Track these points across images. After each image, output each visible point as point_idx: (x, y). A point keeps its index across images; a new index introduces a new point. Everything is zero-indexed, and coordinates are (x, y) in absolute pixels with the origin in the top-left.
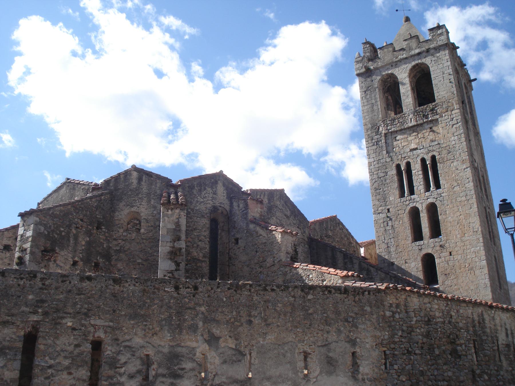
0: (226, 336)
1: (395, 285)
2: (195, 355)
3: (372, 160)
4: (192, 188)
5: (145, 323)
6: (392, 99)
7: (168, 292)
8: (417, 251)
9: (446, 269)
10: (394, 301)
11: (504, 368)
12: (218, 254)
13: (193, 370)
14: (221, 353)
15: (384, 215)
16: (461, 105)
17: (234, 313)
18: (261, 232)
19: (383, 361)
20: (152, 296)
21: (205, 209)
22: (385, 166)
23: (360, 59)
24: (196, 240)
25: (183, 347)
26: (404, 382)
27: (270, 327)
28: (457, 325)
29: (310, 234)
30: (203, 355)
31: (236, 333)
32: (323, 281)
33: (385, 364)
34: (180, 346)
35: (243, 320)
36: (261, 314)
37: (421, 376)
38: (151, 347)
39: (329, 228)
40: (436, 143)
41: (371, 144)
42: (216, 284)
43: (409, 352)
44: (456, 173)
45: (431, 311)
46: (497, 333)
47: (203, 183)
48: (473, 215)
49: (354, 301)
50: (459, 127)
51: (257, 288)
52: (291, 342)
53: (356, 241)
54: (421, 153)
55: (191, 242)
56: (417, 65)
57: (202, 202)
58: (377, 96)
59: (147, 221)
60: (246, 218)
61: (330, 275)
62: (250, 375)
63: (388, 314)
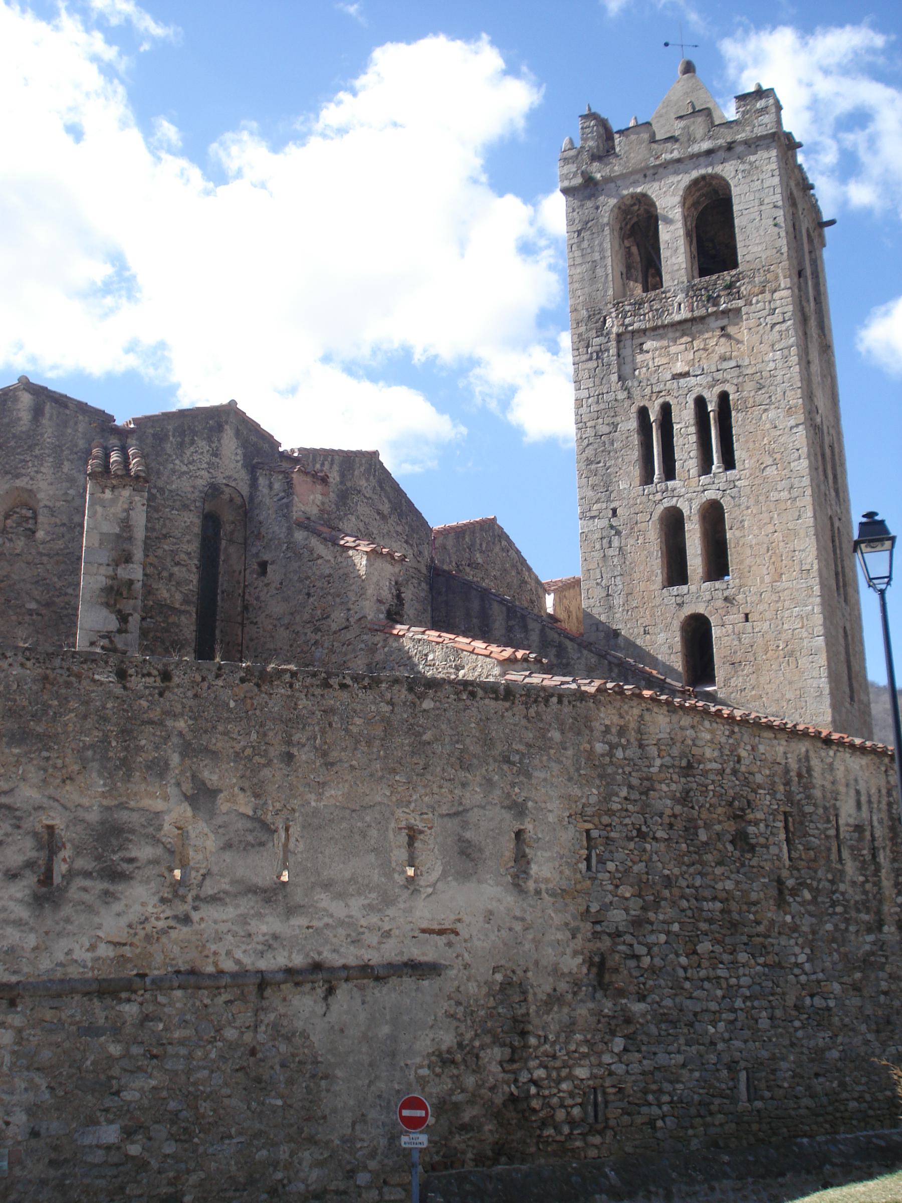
0: (233, 788)
1: (618, 685)
2: (160, 828)
3: (585, 394)
4: (161, 438)
5: (45, 754)
6: (640, 254)
7: (102, 683)
8: (673, 608)
9: (735, 652)
10: (616, 719)
11: (848, 878)
12: (219, 598)
13: (155, 862)
14: (220, 827)
15: (604, 523)
16: (796, 279)
17: (254, 736)
18: (321, 549)
19: (584, 852)
20: (63, 691)
21: (190, 489)
22: (613, 409)
23: (573, 153)
24: (168, 562)
25: (132, 810)
26: (627, 899)
27: (335, 769)
28: (751, 778)
29: (432, 559)
30: (179, 828)
31: (255, 780)
32: (458, 668)
33: (588, 859)
34: (127, 808)
35: (273, 752)
36: (315, 739)
37: (666, 887)
38: (60, 808)
39: (478, 546)
40: (733, 363)
41: (585, 357)
42: (214, 669)
43: (641, 835)
44: (772, 435)
45: (694, 745)
46: (836, 800)
47: (189, 427)
48: (802, 533)
49: (526, 717)
50: (787, 330)
51: (309, 680)
52: (380, 803)
53: (536, 577)
54: (697, 385)
55: (155, 567)
56: (703, 177)
57: (184, 473)
58: (605, 245)
59: (52, 511)
60: (286, 517)
61: (474, 657)
62: (285, 877)
63: (600, 748)
